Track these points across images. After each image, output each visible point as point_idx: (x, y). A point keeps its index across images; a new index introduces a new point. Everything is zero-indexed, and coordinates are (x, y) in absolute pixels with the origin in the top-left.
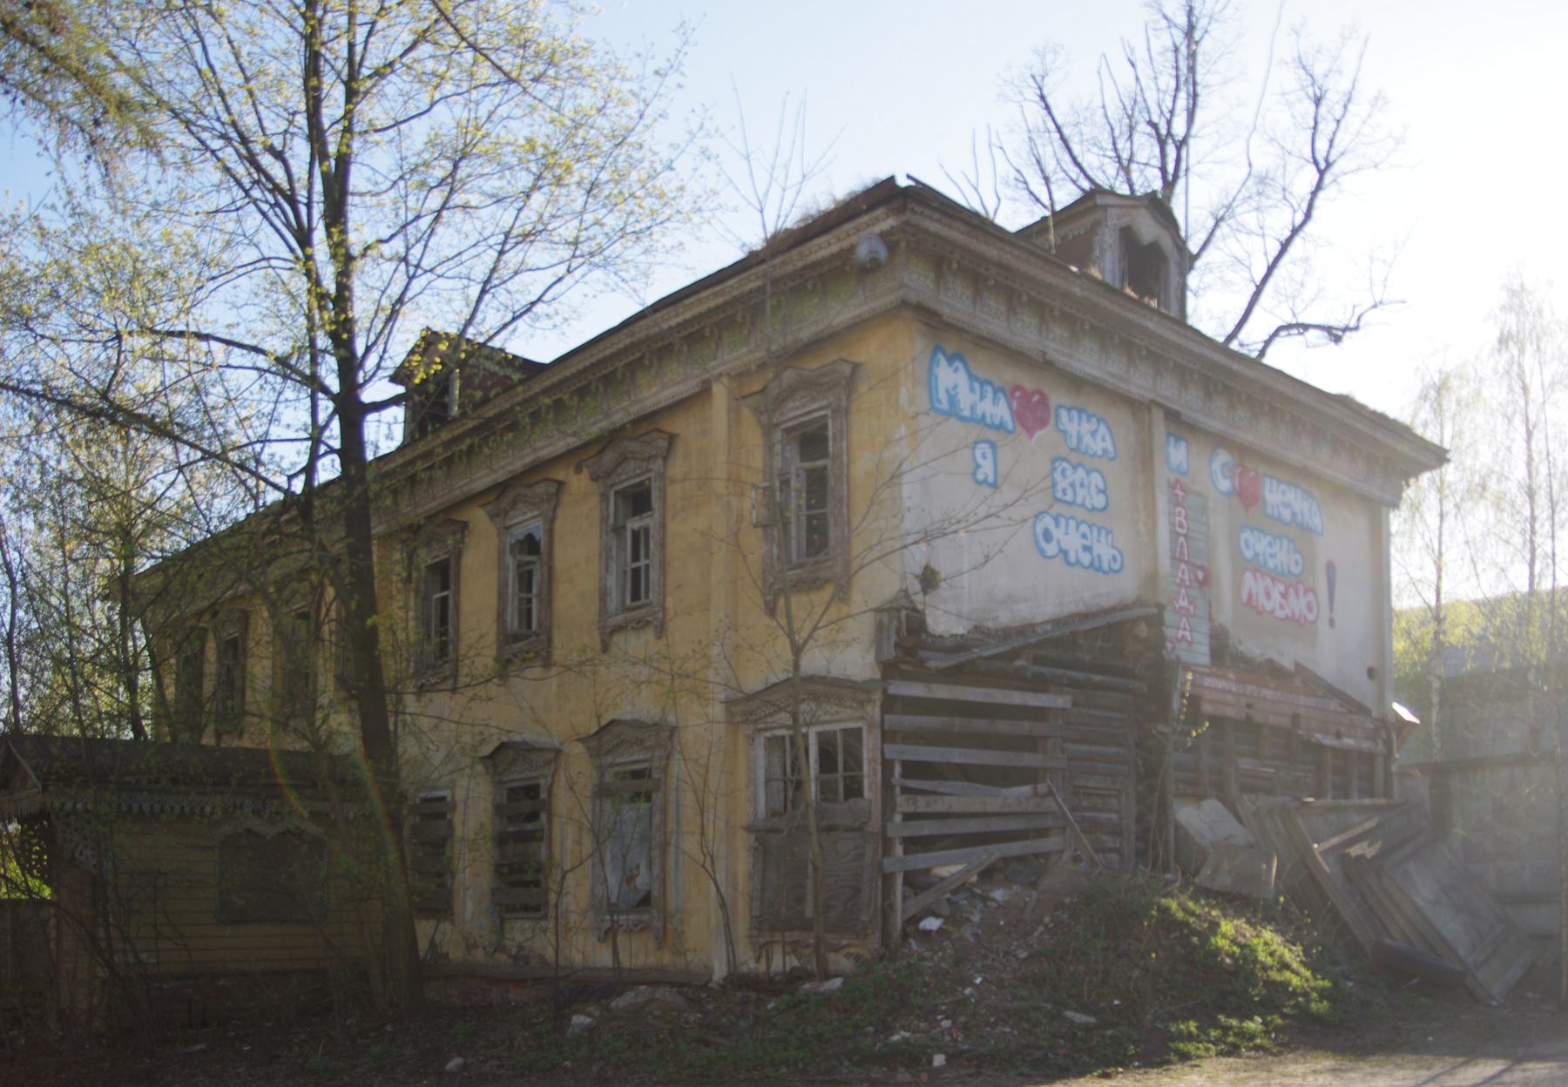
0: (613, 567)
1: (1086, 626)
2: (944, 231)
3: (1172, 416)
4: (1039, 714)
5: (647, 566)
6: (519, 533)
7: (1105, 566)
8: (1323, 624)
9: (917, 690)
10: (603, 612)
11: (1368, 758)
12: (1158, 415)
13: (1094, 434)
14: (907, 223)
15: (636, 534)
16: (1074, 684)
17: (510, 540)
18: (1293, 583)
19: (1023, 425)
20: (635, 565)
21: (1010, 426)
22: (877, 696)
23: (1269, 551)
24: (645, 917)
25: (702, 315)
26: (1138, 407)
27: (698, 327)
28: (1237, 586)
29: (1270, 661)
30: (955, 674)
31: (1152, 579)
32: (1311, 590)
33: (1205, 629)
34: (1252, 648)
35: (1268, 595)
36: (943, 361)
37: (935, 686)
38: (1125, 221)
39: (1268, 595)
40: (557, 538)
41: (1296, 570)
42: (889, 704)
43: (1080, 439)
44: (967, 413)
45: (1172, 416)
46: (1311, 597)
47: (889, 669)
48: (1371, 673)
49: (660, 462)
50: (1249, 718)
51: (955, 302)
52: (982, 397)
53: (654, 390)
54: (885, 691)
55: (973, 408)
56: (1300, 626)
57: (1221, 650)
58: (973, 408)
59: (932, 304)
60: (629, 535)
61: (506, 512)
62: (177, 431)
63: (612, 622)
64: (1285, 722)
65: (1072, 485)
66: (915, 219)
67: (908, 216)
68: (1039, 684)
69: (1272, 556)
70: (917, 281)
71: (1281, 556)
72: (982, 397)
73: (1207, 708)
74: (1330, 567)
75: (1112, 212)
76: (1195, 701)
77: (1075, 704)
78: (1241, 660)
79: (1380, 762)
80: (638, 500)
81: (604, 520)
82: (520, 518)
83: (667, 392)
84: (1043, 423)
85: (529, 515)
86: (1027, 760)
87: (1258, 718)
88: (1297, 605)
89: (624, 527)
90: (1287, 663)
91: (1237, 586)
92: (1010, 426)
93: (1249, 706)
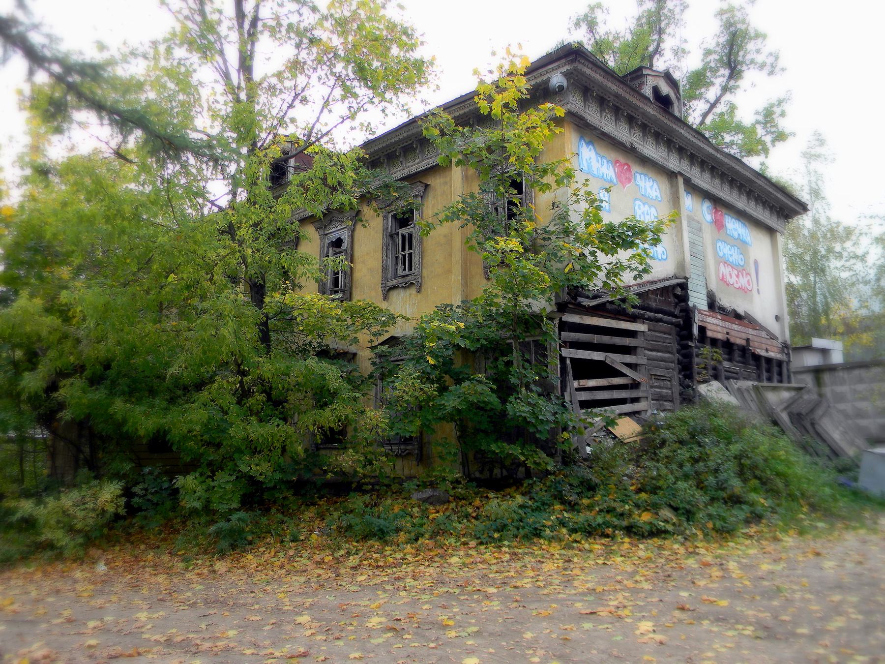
0: (390, 254)
1: (654, 287)
2: (593, 74)
3: (688, 182)
4: (632, 334)
5: (411, 255)
6: (333, 237)
7: (660, 257)
8: (755, 292)
9: (575, 319)
10: (385, 279)
11: (780, 363)
12: (680, 181)
13: (651, 187)
14: (576, 69)
15: (403, 237)
16: (649, 319)
17: (327, 241)
18: (741, 270)
19: (621, 181)
20: (403, 253)
21: (615, 181)
22: (557, 322)
23: (729, 253)
24: (409, 447)
25: (396, 142)
26: (671, 175)
27: (410, 142)
28: (717, 270)
29: (734, 310)
30: (600, 310)
31: (681, 265)
32: (748, 274)
33: (704, 292)
34: (725, 301)
35: (731, 275)
36: (584, 145)
37: (584, 317)
38: (654, 83)
39: (731, 275)
40: (356, 239)
41: (742, 263)
42: (564, 326)
43: (645, 189)
44: (596, 173)
45: (688, 182)
46: (749, 277)
47: (562, 307)
48: (777, 318)
49: (420, 199)
50: (728, 340)
51: (593, 115)
52: (602, 165)
53: (417, 161)
54: (561, 319)
55: (598, 170)
56: (745, 291)
57: (712, 305)
58: (598, 170)
59: (582, 113)
60: (400, 236)
61: (326, 226)
62: (282, 114)
63: (390, 284)
64: (743, 343)
65: (643, 213)
66: (580, 67)
67: (576, 64)
68: (633, 318)
69: (731, 255)
70: (576, 103)
71: (734, 256)
72: (602, 165)
73: (709, 334)
74: (756, 263)
75: (649, 78)
76: (702, 329)
77: (649, 330)
78: (722, 310)
79: (785, 365)
80: (404, 220)
81: (385, 230)
82: (334, 230)
83: (422, 164)
84: (630, 180)
85: (339, 228)
86: (616, 360)
87: (732, 340)
88: (743, 281)
89: (397, 234)
90: (741, 311)
91: (717, 270)
92: (615, 181)
93: (728, 333)
